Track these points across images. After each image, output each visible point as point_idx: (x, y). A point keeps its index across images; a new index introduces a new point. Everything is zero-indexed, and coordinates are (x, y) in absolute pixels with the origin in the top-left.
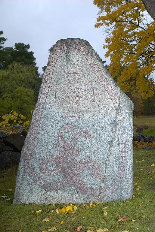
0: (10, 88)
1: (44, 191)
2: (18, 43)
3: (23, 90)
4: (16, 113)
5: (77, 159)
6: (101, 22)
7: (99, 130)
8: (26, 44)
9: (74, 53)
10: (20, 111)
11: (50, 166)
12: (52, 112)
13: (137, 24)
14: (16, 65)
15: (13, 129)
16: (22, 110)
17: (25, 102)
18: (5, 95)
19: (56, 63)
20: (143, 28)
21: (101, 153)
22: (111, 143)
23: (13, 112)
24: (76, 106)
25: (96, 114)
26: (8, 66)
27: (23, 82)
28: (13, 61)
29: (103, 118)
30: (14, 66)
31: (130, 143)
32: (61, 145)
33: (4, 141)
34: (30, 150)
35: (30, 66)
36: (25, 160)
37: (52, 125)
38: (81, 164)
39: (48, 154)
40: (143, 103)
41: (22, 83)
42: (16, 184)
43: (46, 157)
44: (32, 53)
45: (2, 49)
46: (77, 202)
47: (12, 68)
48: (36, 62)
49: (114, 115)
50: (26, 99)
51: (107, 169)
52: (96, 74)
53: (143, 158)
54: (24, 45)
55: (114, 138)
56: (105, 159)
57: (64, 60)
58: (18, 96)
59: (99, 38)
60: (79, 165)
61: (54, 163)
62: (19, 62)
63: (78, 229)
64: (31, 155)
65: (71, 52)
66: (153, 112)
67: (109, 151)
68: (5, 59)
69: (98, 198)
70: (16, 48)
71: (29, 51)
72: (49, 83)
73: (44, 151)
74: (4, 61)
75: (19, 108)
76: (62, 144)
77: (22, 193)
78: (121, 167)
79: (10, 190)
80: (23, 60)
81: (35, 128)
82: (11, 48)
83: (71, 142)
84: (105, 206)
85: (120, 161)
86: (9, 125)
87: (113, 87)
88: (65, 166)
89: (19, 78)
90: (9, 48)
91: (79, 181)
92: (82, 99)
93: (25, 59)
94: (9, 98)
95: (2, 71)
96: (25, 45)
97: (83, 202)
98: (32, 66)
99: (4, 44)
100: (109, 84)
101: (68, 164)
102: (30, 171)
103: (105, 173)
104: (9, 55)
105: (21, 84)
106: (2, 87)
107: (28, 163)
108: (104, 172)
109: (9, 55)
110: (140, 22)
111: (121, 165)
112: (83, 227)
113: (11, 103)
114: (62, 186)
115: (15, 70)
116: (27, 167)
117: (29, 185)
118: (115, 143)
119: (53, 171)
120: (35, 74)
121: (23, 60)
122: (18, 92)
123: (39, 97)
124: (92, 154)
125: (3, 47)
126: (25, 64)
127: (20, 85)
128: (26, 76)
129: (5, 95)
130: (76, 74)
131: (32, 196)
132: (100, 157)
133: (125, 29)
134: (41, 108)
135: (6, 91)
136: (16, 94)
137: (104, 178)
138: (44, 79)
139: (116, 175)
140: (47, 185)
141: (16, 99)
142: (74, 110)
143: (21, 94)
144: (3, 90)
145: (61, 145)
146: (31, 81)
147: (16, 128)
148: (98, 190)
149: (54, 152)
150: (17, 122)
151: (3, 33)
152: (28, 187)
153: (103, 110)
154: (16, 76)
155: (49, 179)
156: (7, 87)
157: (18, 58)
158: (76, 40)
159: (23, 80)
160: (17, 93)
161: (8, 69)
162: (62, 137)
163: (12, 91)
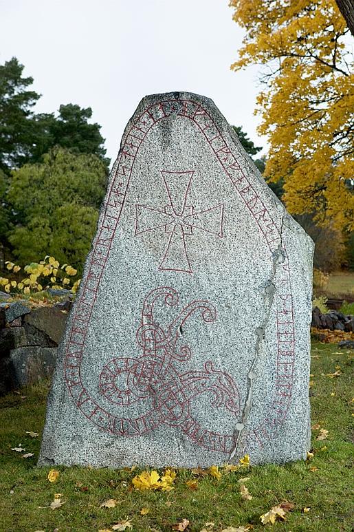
0: (47, 205)
1: (106, 437)
2: (65, 105)
3: (76, 209)
4: (56, 260)
5: (183, 367)
6: (246, 56)
7: (233, 302)
8: (83, 106)
10: (68, 255)
11: (123, 381)
12: (127, 260)
13: (331, 64)
14: (60, 152)
15: (46, 297)
16: (73, 255)
17: (80, 236)
18: (35, 222)
19: (138, 148)
20: (344, 73)
21: (237, 354)
22: (261, 332)
23: (48, 258)
26: (42, 156)
27: (76, 191)
28: (54, 144)
29: (243, 274)
30: (57, 156)
31: (304, 332)
32: (148, 334)
35: (93, 155)
36: (66, 366)
37: (129, 288)
39: (116, 354)
40: (346, 243)
41: (74, 194)
42: (45, 422)
43: (114, 361)
45: (29, 117)
46: (181, 464)
47: (53, 161)
48: (105, 148)
49: (270, 268)
50: (81, 230)
51: (250, 391)
52: (229, 175)
53: (338, 367)
54: (79, 108)
55: (267, 320)
57: (155, 142)
58: (64, 223)
59: (244, 96)
61: (131, 375)
62: (69, 146)
63: (181, 527)
64: (80, 356)
65: (174, 123)
66: (311, 249)
67: (257, 349)
68: (36, 141)
70: (61, 116)
71: (90, 121)
72: (123, 192)
74: (34, 145)
75: (65, 250)
76: (150, 332)
77: (58, 442)
78: (283, 386)
79: (34, 434)
80: (76, 142)
81: (90, 296)
82: (49, 115)
84: (244, 474)
86: (40, 287)
87: (268, 205)
88: (156, 382)
89: (66, 183)
90: (46, 115)
91: (186, 418)
92: (195, 231)
93: (82, 140)
94: (44, 227)
95: (30, 167)
96: (81, 109)
97: (195, 464)
98: (97, 156)
99: (35, 106)
100: (257, 197)
102: (76, 392)
103: (246, 400)
104: (46, 131)
105: (70, 196)
106: (30, 202)
109: (46, 131)
110: (338, 61)
111: (284, 383)
112: (190, 523)
113: (47, 240)
115: (57, 166)
116: (69, 383)
117: (74, 423)
118: (270, 332)
119: (128, 393)
120: (102, 175)
121: (76, 142)
122: (64, 213)
123: (100, 225)
125: (32, 113)
126: (82, 151)
127: (69, 197)
128: (83, 178)
129: (35, 221)
130: (184, 172)
131: (81, 450)
132: (234, 364)
133: (305, 76)
135: (37, 212)
136: (60, 219)
137: (243, 412)
138: (111, 185)
139: (272, 405)
141: (60, 229)
142: (178, 255)
143: (71, 219)
144: (30, 208)
145: (148, 334)
146: (92, 191)
147: (55, 294)
148: (231, 438)
149: (132, 351)
150: (59, 282)
151: (34, 82)
152: (71, 428)
154: (60, 179)
155: (120, 411)
156: (40, 203)
157: (67, 138)
158: (184, 97)
159: (76, 188)
160: (63, 216)
161: (42, 162)
162: (149, 316)
163: (50, 211)
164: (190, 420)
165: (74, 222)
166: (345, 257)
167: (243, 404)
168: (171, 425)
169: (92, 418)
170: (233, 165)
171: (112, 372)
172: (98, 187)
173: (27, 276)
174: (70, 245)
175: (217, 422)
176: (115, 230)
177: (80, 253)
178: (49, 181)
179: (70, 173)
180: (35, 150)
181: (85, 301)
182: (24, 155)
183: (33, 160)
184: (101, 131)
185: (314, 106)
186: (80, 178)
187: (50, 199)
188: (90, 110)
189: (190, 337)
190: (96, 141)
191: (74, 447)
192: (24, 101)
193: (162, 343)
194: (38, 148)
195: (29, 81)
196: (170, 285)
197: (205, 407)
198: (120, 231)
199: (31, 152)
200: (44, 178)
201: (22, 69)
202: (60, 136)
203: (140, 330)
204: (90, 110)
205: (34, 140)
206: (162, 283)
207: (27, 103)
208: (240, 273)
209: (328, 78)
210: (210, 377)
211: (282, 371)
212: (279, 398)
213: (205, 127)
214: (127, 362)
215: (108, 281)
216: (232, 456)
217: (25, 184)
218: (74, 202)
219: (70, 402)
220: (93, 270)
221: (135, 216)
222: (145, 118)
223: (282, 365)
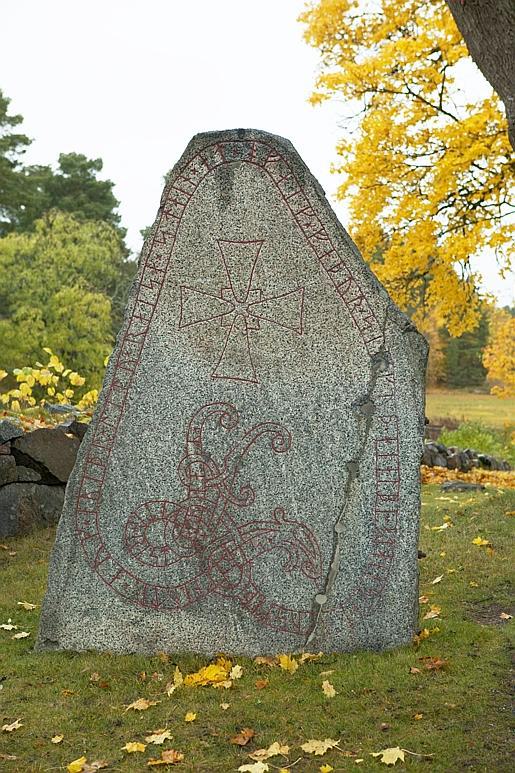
0: (40, 290)
5: (244, 515)
6: (324, 90)
7: (316, 425)
8: (91, 157)
9: (246, 181)
12: (167, 363)
14: (59, 218)
16: (74, 360)
17: (85, 333)
22: (353, 467)
26: (34, 222)
27: (80, 271)
30: (55, 223)
34: (96, 481)
35: (103, 223)
40: (444, 350)
43: (146, 504)
44: (108, 185)
49: (367, 379)
50: (86, 324)
51: (337, 551)
53: (446, 518)
54: (85, 158)
55: (362, 451)
57: (211, 197)
58: (62, 315)
62: (71, 210)
64: (98, 496)
70: (61, 168)
71: (100, 177)
76: (198, 465)
80: (80, 205)
83: (225, 460)
86: (33, 401)
88: (204, 536)
94: (34, 319)
96: (88, 160)
99: (24, 154)
100: (351, 278)
101: (213, 529)
104: (39, 189)
107: (87, 523)
108: (328, 558)
109: (39, 189)
113: (39, 337)
115: (54, 236)
117: (88, 591)
118: (365, 469)
119: (164, 549)
120: (116, 250)
123: (128, 315)
124: (291, 499)
126: (88, 217)
127: (70, 280)
129: (22, 311)
131: (98, 629)
135: (26, 299)
139: (366, 569)
141: (56, 323)
143: (72, 310)
144: (17, 294)
149: (171, 491)
154: (57, 255)
155: (152, 575)
157: (68, 199)
159: (80, 268)
161: (33, 230)
162: (198, 444)
164: (252, 588)
165: (76, 315)
166: (442, 368)
167: (326, 568)
172: (110, 267)
173: (16, 385)
174: (70, 346)
176: (150, 322)
177: (83, 356)
178: (42, 257)
179: (71, 246)
180: (24, 214)
181: (106, 421)
182: (8, 221)
183: (20, 228)
184: (114, 191)
185: (409, 161)
186: (85, 254)
187: (44, 282)
188: (100, 161)
189: (252, 472)
190: (109, 204)
192: (11, 148)
193: (215, 481)
194: (27, 213)
195: (17, 120)
199: (18, 216)
200: (35, 253)
201: (8, 103)
202: (59, 195)
204: (100, 161)
205: (23, 200)
207: (14, 150)
209: (430, 124)
210: (281, 529)
211: (381, 522)
212: (376, 560)
215: (140, 393)
216: (310, 639)
217: (10, 260)
218: (77, 286)
222: (195, 164)
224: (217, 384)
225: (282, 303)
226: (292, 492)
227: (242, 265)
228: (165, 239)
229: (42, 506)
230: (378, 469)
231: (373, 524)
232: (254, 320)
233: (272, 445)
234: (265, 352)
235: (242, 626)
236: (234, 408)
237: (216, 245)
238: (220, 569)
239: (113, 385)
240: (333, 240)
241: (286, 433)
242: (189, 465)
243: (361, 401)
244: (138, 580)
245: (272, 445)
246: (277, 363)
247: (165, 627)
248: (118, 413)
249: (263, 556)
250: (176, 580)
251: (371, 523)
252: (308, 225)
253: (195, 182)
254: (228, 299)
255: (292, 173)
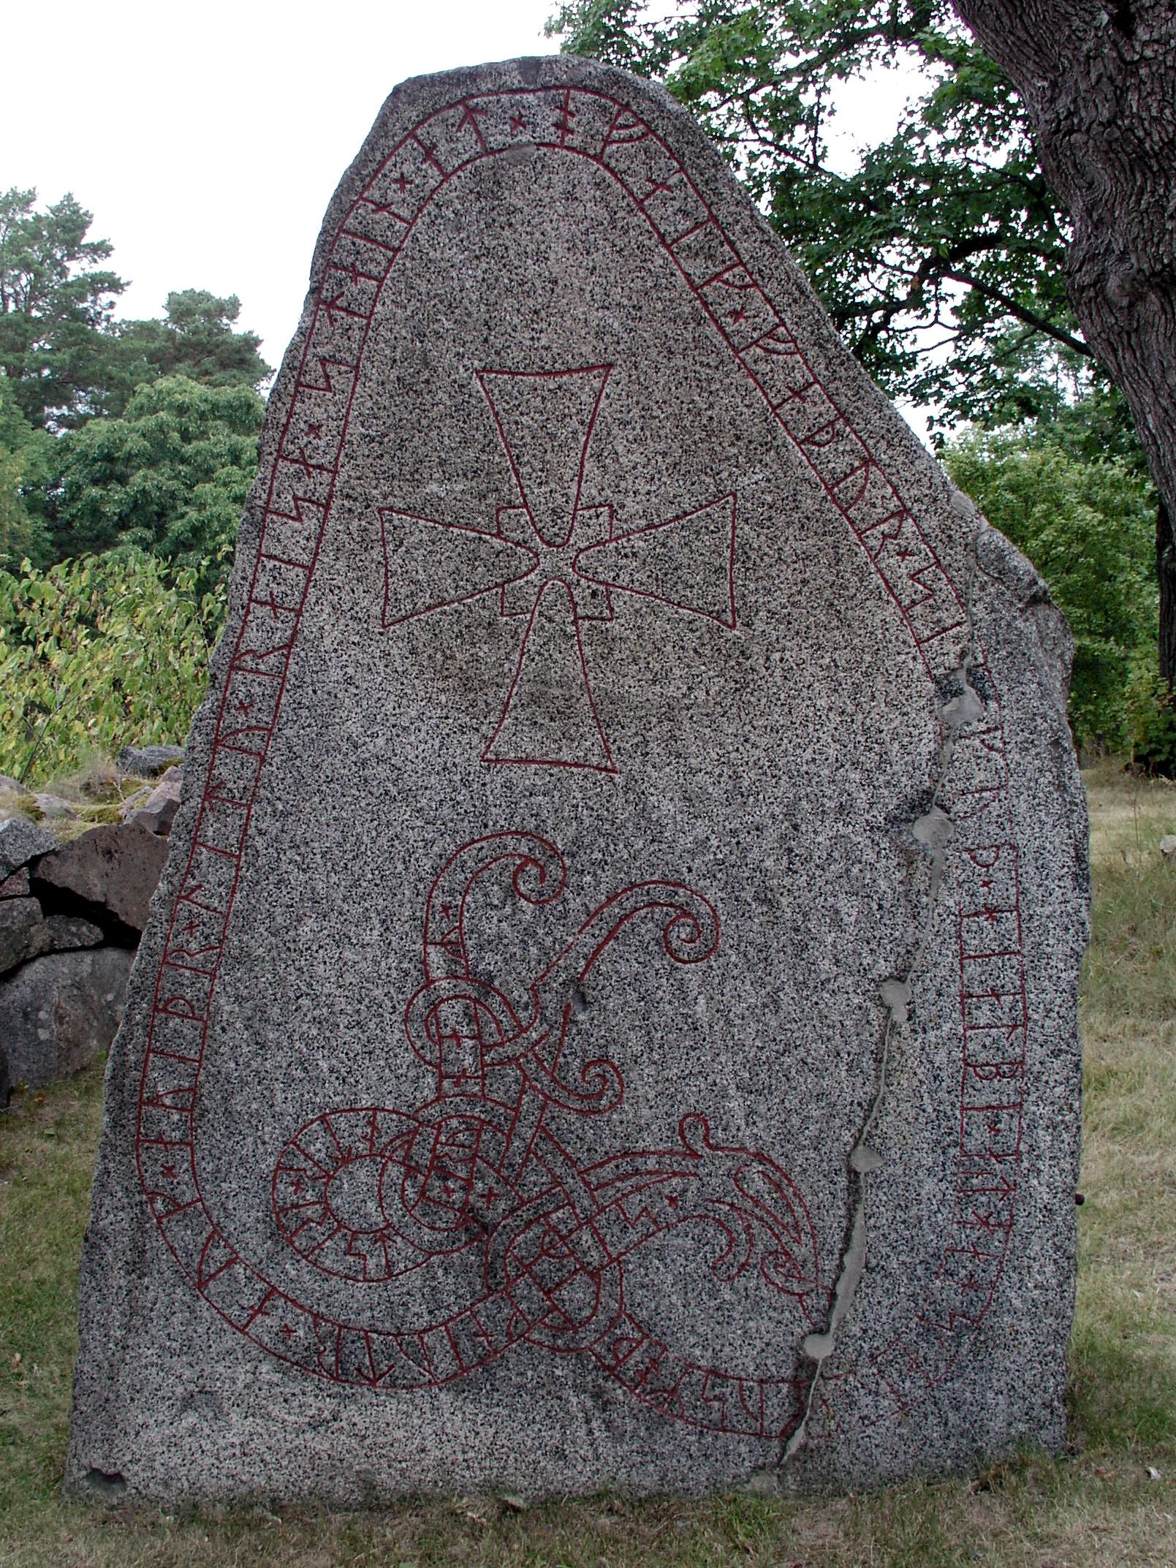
8: (221, 292)
12: (354, 728)
21: (807, 1083)
24: (575, 669)
25: (763, 742)
32: (451, 1013)
33: (40, 888)
34: (183, 1059)
38: (627, 1176)
39: (332, 1094)
51: (859, 1220)
56: (847, 1137)
60: (610, 1183)
64: (191, 1101)
69: (784, 1449)
71: (238, 328)
73: (299, 1074)
76: (459, 1007)
83: (534, 991)
85: (971, 1145)
88: (489, 1196)
91: (613, 1322)
100: (868, 461)
101: (513, 1181)
103: (843, 1252)
107: (169, 1171)
108: (836, 1239)
114: (469, 1357)
116: (159, 1205)
118: (931, 996)
119: (382, 1236)
124: (725, 1089)
130: (569, 371)
131: (222, 1442)
132: (795, 1120)
134: (257, 690)
139: (940, 1263)
140: (337, 1350)
142: (560, 703)
145: (451, 1013)
149: (389, 1079)
152: (177, 1364)
153: (822, 703)
155: (356, 1302)
162: (455, 949)
164: (627, 1328)
167: (829, 1264)
168: (554, 1349)
169: (252, 1330)
170: (769, 334)
171: (316, 1164)
175: (734, 1333)
176: (299, 614)
181: (198, 896)
189: (613, 1021)
191: (193, 1431)
193: (509, 1049)
195: (101, 249)
196: (531, 824)
197: (684, 1281)
198: (319, 618)
203: (420, 1001)
206: (498, 816)
208: (813, 768)
210: (702, 1171)
211: (979, 1138)
212: (965, 1238)
213: (650, 187)
214: (371, 1123)
219: (168, 1274)
220: (223, 772)
221: (376, 554)
223: (979, 1117)
224: (499, 780)
225: (674, 541)
226: (726, 1070)
227: (553, 437)
228: (327, 377)
229: (110, 997)
230: (966, 996)
231: (956, 1144)
232: (594, 594)
233: (664, 943)
234: (631, 685)
235: (608, 1425)
236: (552, 846)
237: (476, 384)
238: (539, 1281)
239: (208, 795)
240: (812, 353)
241: (704, 909)
242: (434, 1007)
243: (912, 809)
244: (317, 1316)
245: (664, 943)
246: (669, 713)
247: (399, 1434)
248: (227, 873)
249: (655, 1242)
250: (419, 1315)
251: (949, 1140)
252: (736, 314)
253: (405, 213)
254: (517, 536)
255: (682, 169)
